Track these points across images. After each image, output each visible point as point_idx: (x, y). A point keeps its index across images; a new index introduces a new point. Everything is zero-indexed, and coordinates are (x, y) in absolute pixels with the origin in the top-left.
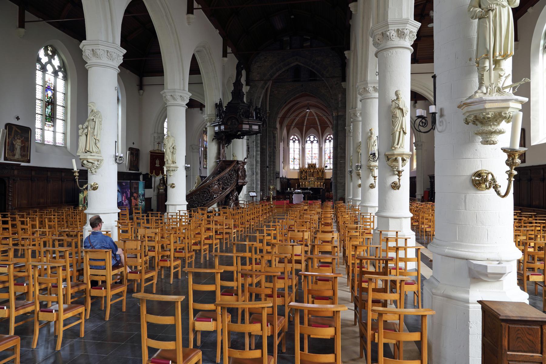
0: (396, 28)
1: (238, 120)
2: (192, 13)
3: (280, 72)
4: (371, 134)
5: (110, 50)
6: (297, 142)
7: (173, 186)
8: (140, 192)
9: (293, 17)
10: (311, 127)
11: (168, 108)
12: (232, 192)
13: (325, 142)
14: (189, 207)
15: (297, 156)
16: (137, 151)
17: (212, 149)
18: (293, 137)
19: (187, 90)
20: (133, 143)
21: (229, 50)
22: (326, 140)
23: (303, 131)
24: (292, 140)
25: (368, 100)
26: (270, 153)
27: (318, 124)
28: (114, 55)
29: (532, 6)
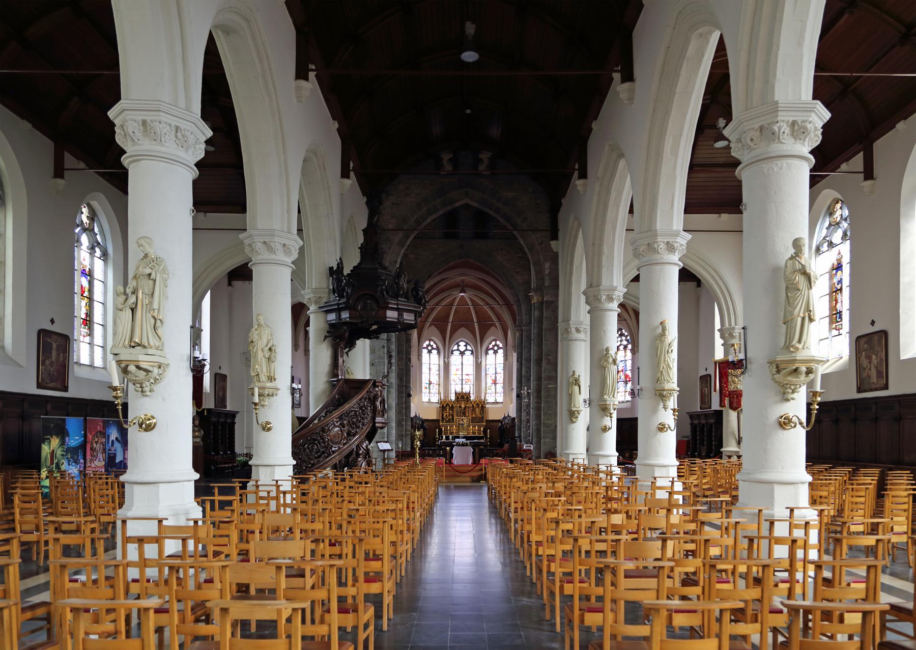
0: (791, 119)
3: (433, 217)
4: (664, 329)
5: (182, 126)
6: (434, 352)
9: (468, 111)
10: (462, 326)
13: (487, 353)
15: (434, 379)
18: (427, 342)
22: (487, 349)
23: (446, 333)
24: (427, 348)
25: (657, 267)
27: (475, 320)
28: (191, 139)
29: (905, 118)
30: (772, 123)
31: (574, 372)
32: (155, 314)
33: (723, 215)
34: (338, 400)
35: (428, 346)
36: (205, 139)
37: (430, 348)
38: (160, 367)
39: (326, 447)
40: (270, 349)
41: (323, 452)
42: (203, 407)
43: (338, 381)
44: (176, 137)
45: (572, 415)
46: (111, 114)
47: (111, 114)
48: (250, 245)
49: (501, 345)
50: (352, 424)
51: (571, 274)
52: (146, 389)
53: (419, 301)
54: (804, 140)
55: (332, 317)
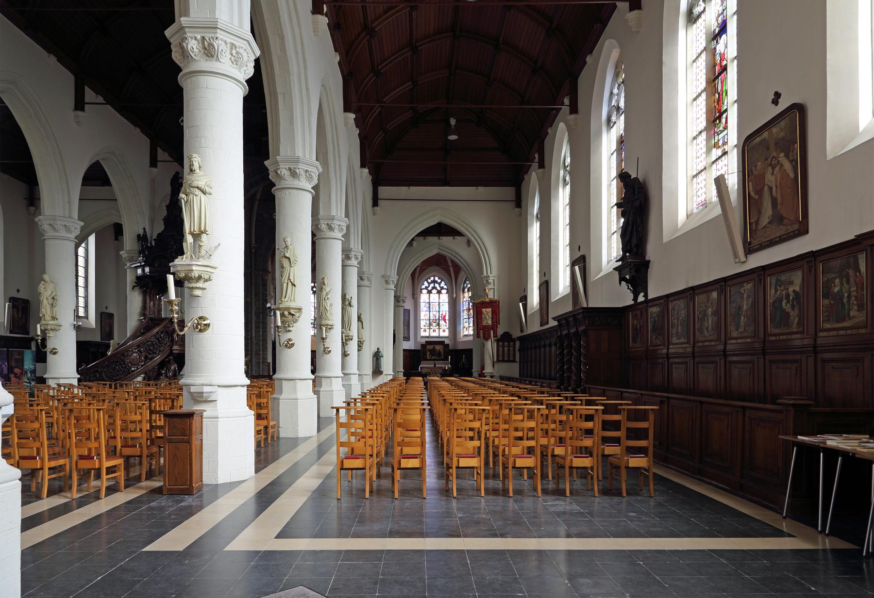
2: (83, 109)
7: (54, 352)
8: (26, 367)
11: (47, 242)
17: (135, 301)
19: (76, 217)
20: (18, 291)
33: (480, 188)
44: (232, 54)
46: (168, 33)
47: (168, 33)
50: (148, 351)
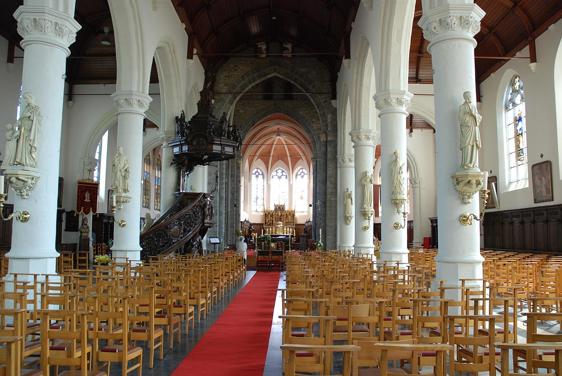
0: (459, 15)
1: (207, 140)
3: (253, 84)
4: (397, 157)
5: (60, 23)
6: (261, 176)
9: (274, 18)
12: (193, 238)
14: (144, 256)
15: (260, 196)
16: (62, 178)
21: (195, 51)
22: (297, 175)
26: (233, 188)
27: (288, 155)
30: (446, 17)
31: (347, 189)
32: (31, 143)
34: (179, 207)
35: (256, 173)
36: (76, 31)
37: (257, 174)
38: (33, 179)
39: (169, 240)
40: (126, 170)
41: (166, 243)
42: (97, 212)
43: (180, 193)
44: (56, 29)
45: (347, 219)
46: (15, 15)
47: (15, 15)
48: (117, 101)
49: (306, 172)
51: (344, 122)
52: (23, 194)
53: (236, 139)
54: (469, 28)
55: (176, 150)
